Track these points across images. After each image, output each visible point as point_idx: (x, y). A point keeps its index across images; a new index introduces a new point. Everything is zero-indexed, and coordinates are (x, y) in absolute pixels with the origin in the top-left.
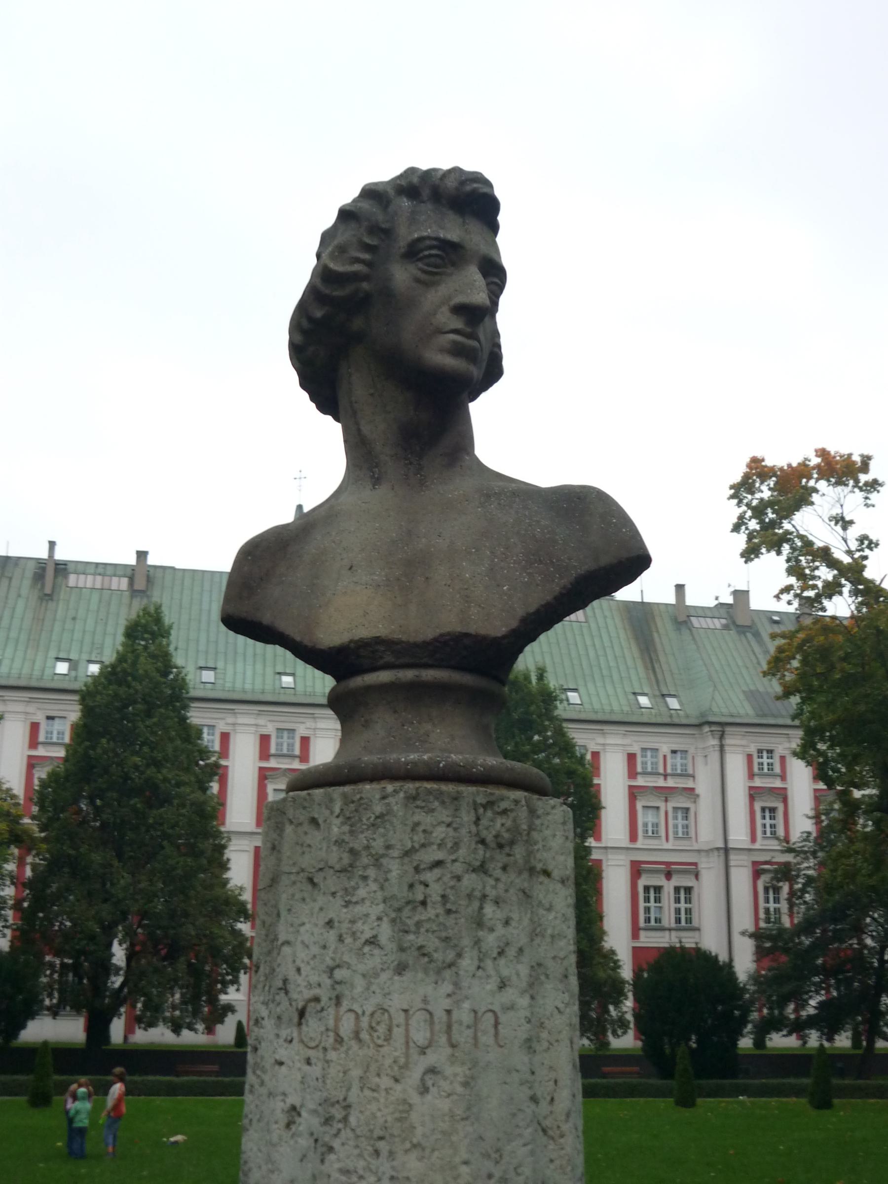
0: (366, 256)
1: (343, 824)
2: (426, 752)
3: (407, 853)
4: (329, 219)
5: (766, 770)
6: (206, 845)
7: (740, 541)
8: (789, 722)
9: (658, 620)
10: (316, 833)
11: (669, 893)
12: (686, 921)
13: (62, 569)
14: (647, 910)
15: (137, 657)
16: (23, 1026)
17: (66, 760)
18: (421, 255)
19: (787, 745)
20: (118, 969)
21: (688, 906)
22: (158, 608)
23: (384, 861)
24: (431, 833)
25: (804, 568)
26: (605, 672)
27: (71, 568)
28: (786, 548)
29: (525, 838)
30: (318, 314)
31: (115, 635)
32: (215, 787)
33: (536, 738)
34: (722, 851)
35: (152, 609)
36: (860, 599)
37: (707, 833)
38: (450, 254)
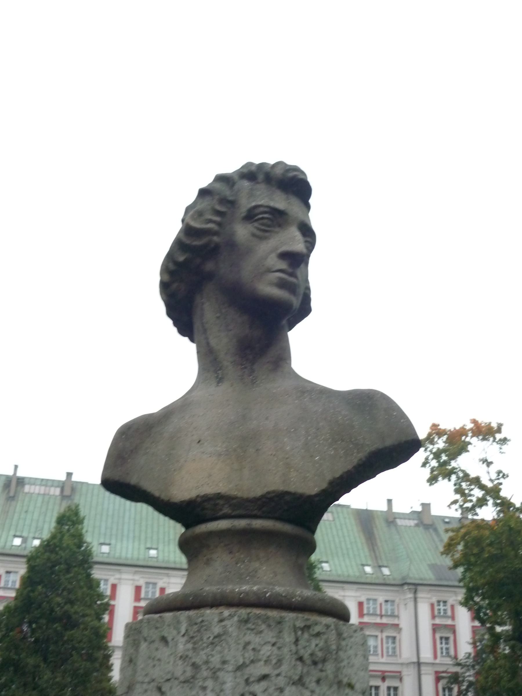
0: (217, 219)
1: (188, 642)
2: (255, 584)
3: (239, 668)
4: (191, 197)
5: (442, 614)
6: (99, 654)
7: (426, 473)
8: (456, 584)
10: (165, 649)
11: (384, 690)
13: (21, 482)
15: (63, 536)
17: (16, 598)
18: (256, 218)
19: (454, 598)
22: (77, 506)
23: (220, 674)
24: (259, 651)
25: (465, 489)
27: (26, 481)
28: (454, 477)
29: (334, 657)
30: (181, 259)
31: (50, 522)
32: (106, 618)
34: (416, 665)
35: (73, 507)
36: (499, 509)
37: (407, 653)
38: (278, 218)
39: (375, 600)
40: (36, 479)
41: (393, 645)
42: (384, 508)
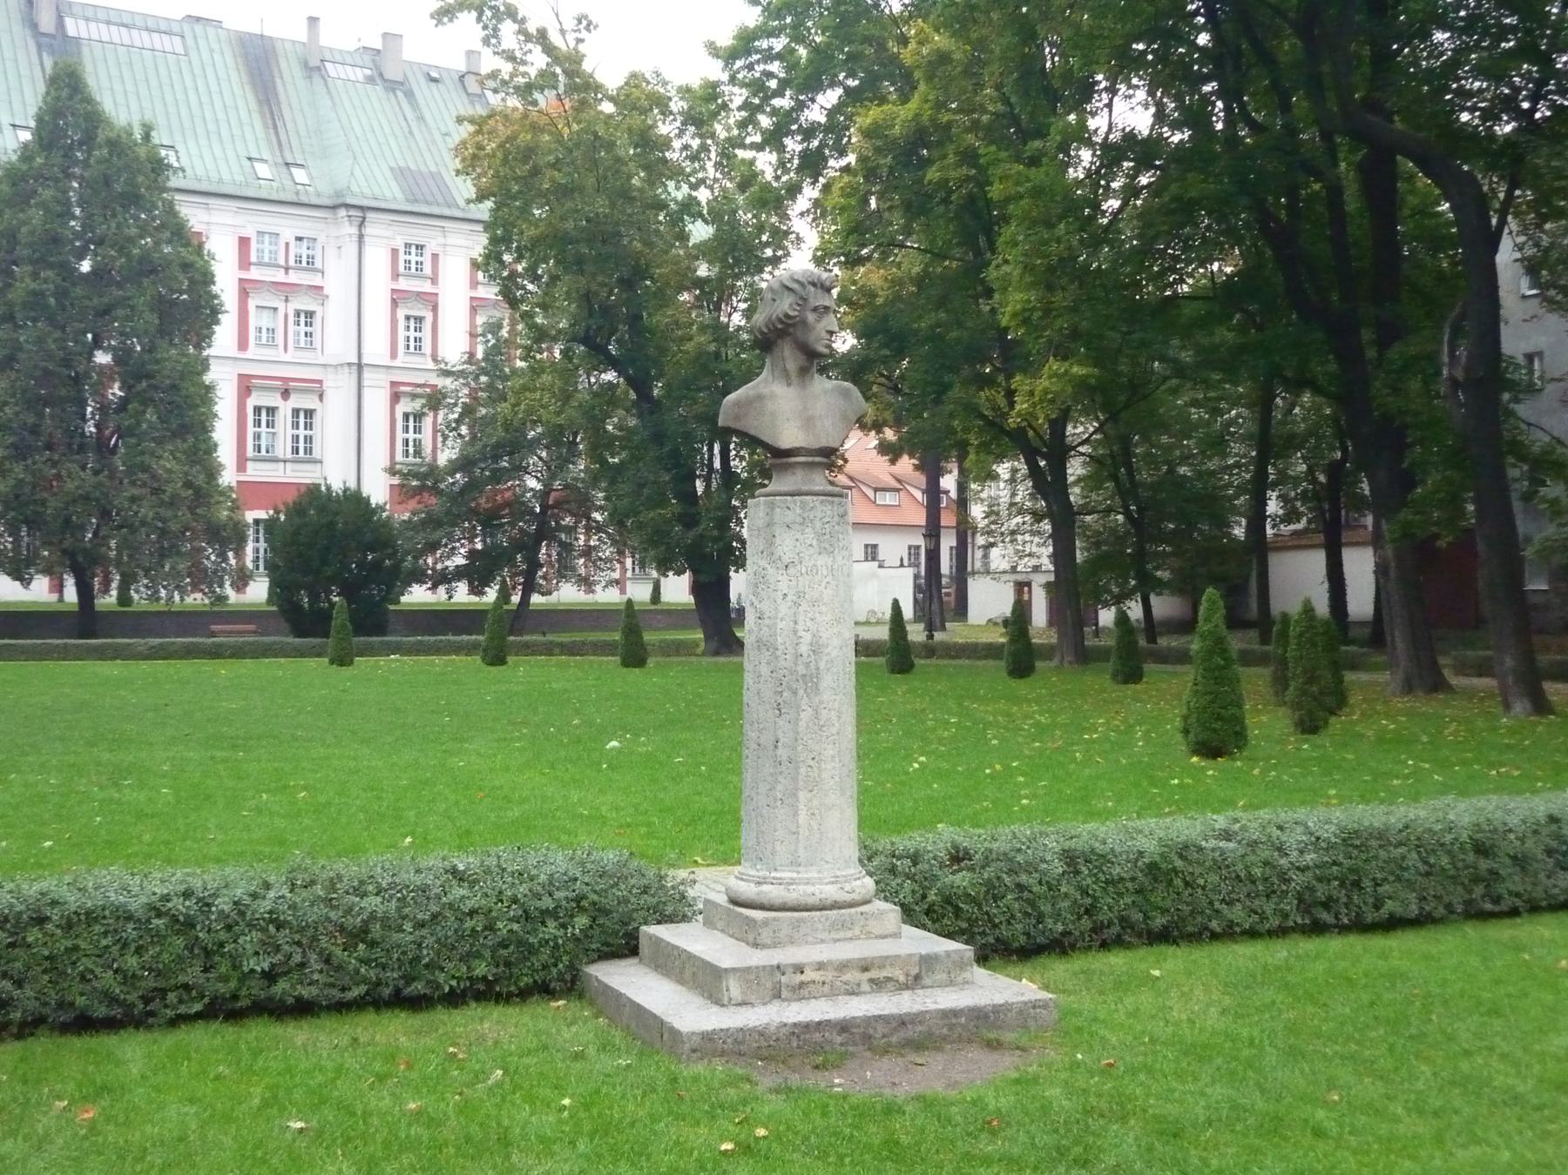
9: (283, 65)
12: (304, 451)
14: (257, 436)
21: (308, 432)
26: (211, 127)
42: (301, 35)
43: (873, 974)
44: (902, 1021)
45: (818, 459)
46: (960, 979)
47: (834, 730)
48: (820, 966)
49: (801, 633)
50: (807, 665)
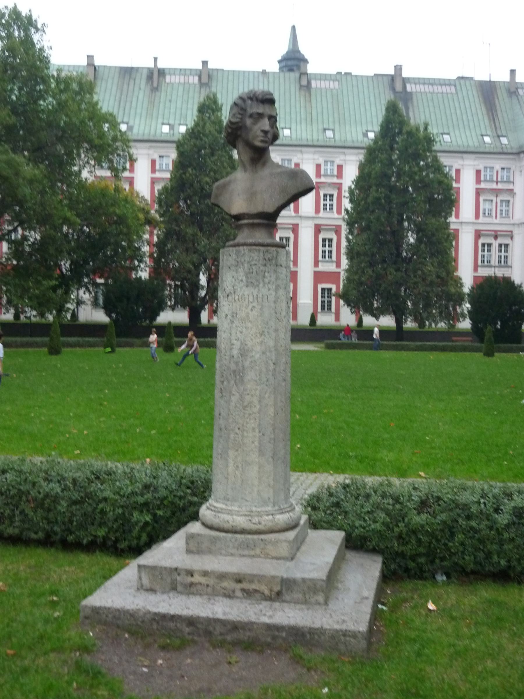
9: (499, 92)
12: (504, 262)
13: (162, 73)
14: (483, 256)
15: (205, 124)
16: (158, 314)
17: (171, 180)
20: (203, 287)
21: (506, 254)
22: (215, 95)
27: (167, 72)
33: (422, 163)
39: (332, 162)
40: (175, 69)
41: (507, 208)
42: (506, 78)
43: (245, 585)
44: (235, 626)
45: (256, 221)
46: (313, 600)
47: (255, 410)
48: (205, 574)
49: (234, 341)
50: (237, 363)
